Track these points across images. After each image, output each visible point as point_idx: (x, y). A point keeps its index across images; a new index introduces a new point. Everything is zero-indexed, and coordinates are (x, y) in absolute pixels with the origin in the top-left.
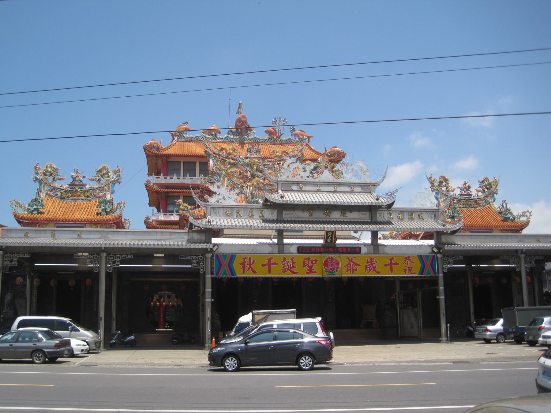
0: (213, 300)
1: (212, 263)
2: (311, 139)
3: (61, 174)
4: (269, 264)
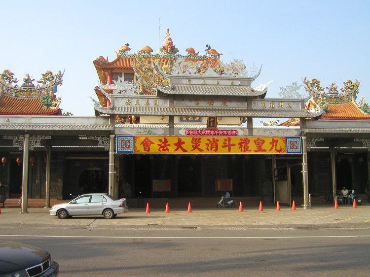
0: (115, 172)
2: (220, 56)
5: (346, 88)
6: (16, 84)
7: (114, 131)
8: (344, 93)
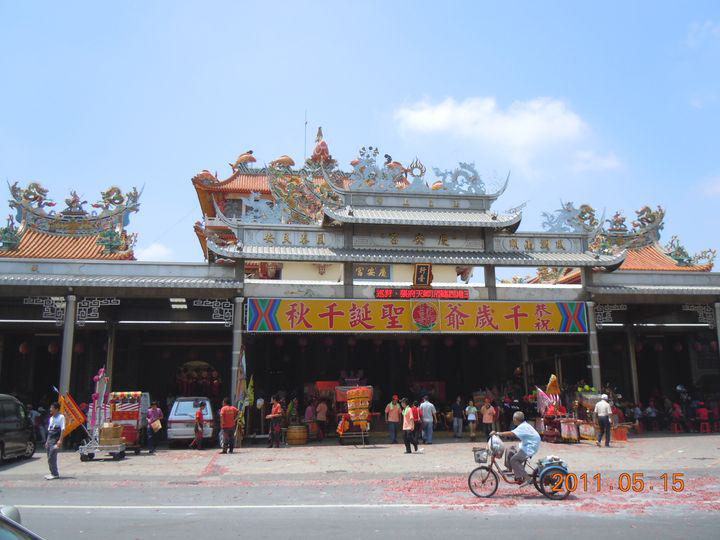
1: (244, 313)
3: (49, 197)
4: (331, 314)
5: (641, 220)
6: (52, 208)
7: (242, 290)
8: (638, 228)
